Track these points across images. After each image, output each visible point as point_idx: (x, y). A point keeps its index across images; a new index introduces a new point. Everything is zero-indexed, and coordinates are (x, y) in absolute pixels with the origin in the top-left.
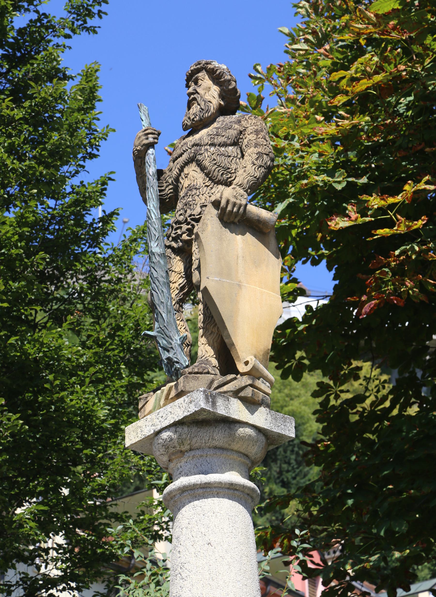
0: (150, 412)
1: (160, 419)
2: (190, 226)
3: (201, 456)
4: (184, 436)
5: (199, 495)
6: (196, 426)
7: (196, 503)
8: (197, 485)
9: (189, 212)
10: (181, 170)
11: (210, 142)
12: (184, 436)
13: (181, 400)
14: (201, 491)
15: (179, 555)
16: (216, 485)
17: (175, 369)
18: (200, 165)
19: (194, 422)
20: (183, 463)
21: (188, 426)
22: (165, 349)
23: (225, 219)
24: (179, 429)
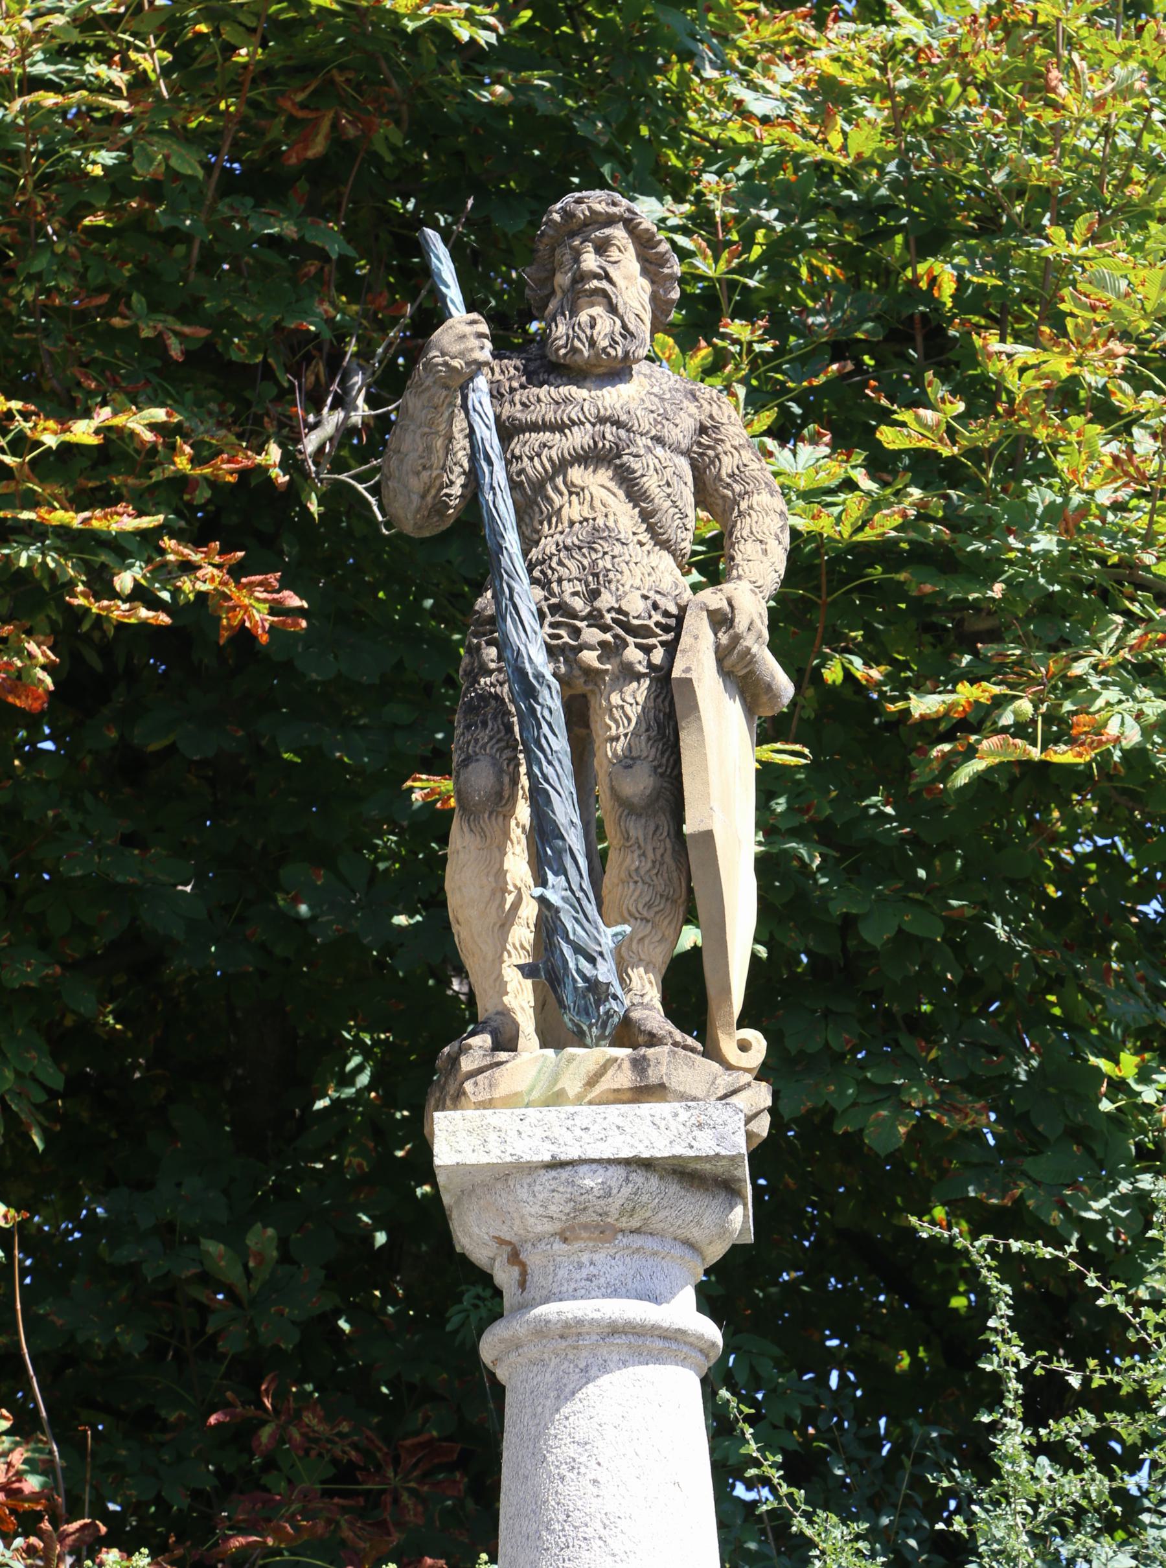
0: (512, 1101)
1: (578, 1132)
2: (608, 637)
3: (655, 1254)
4: (645, 1198)
5: (650, 1353)
6: (680, 1182)
7: (641, 1370)
8: (660, 1328)
9: (606, 600)
10: (561, 466)
11: (653, 433)
12: (645, 1198)
13: (646, 1109)
14: (660, 1344)
15: (595, 1491)
16: (691, 1340)
17: (607, 1013)
18: (628, 482)
19: (674, 1172)
20: (604, 1261)
21: (661, 1178)
22: (578, 950)
23: (728, 663)
24: (638, 1178)
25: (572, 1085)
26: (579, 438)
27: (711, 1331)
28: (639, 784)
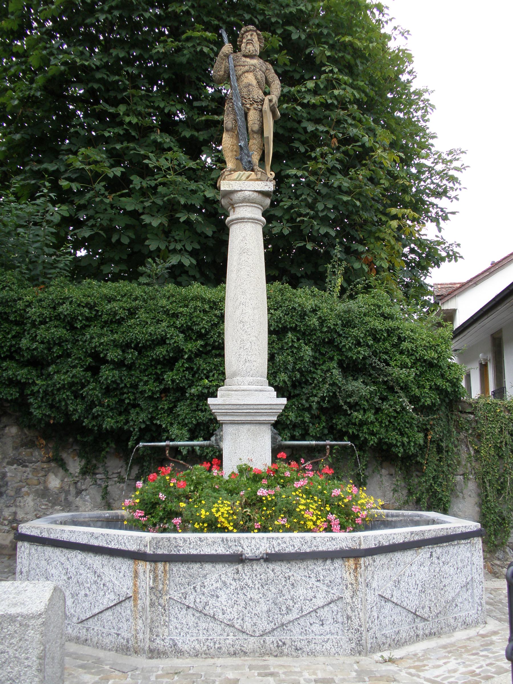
9: (251, 96)
10: (244, 73)
25: (244, 178)
26: (247, 68)
27: (263, 219)
28: (256, 127)
